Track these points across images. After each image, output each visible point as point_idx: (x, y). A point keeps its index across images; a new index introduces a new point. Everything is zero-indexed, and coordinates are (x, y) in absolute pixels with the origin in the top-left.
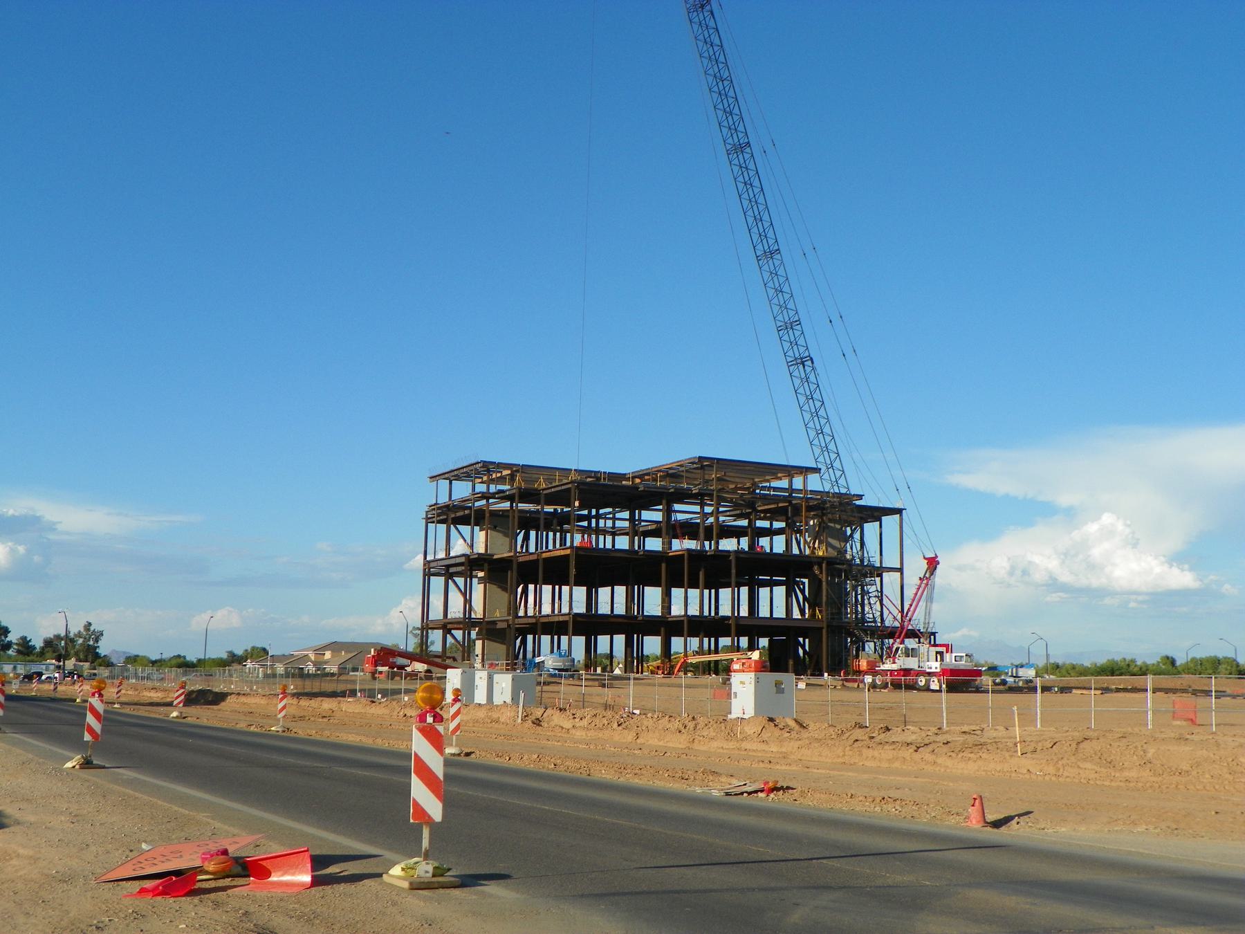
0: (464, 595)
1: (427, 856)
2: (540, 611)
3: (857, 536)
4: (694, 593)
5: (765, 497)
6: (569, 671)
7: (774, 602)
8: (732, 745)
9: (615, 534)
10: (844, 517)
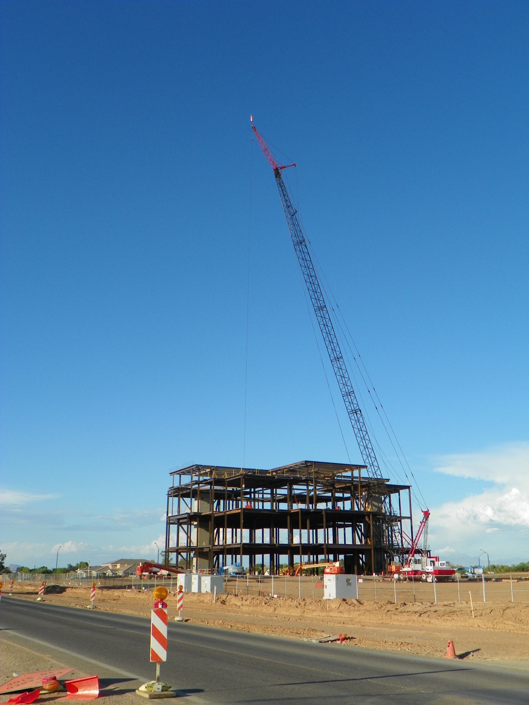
0: (187, 534)
1: (158, 680)
2: (226, 543)
3: (387, 500)
4: (304, 532)
5: (339, 482)
6: (241, 574)
7: (346, 536)
8: (323, 614)
9: (263, 501)
10: (380, 491)
